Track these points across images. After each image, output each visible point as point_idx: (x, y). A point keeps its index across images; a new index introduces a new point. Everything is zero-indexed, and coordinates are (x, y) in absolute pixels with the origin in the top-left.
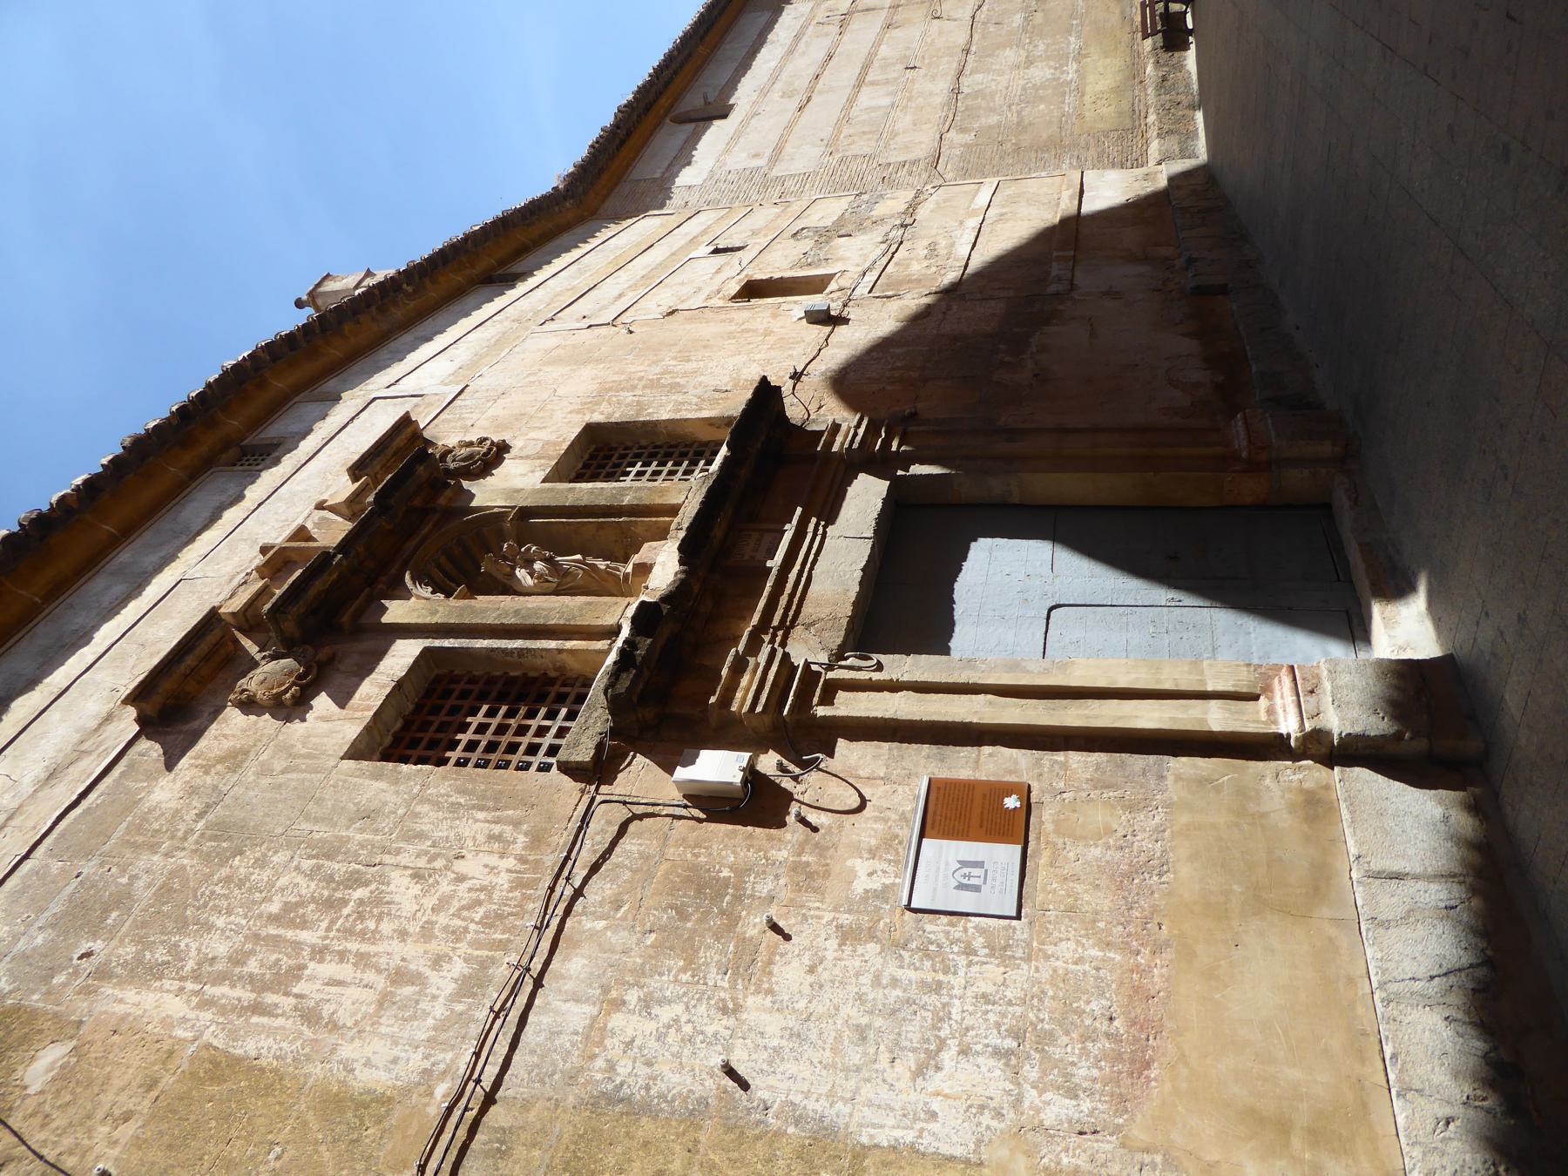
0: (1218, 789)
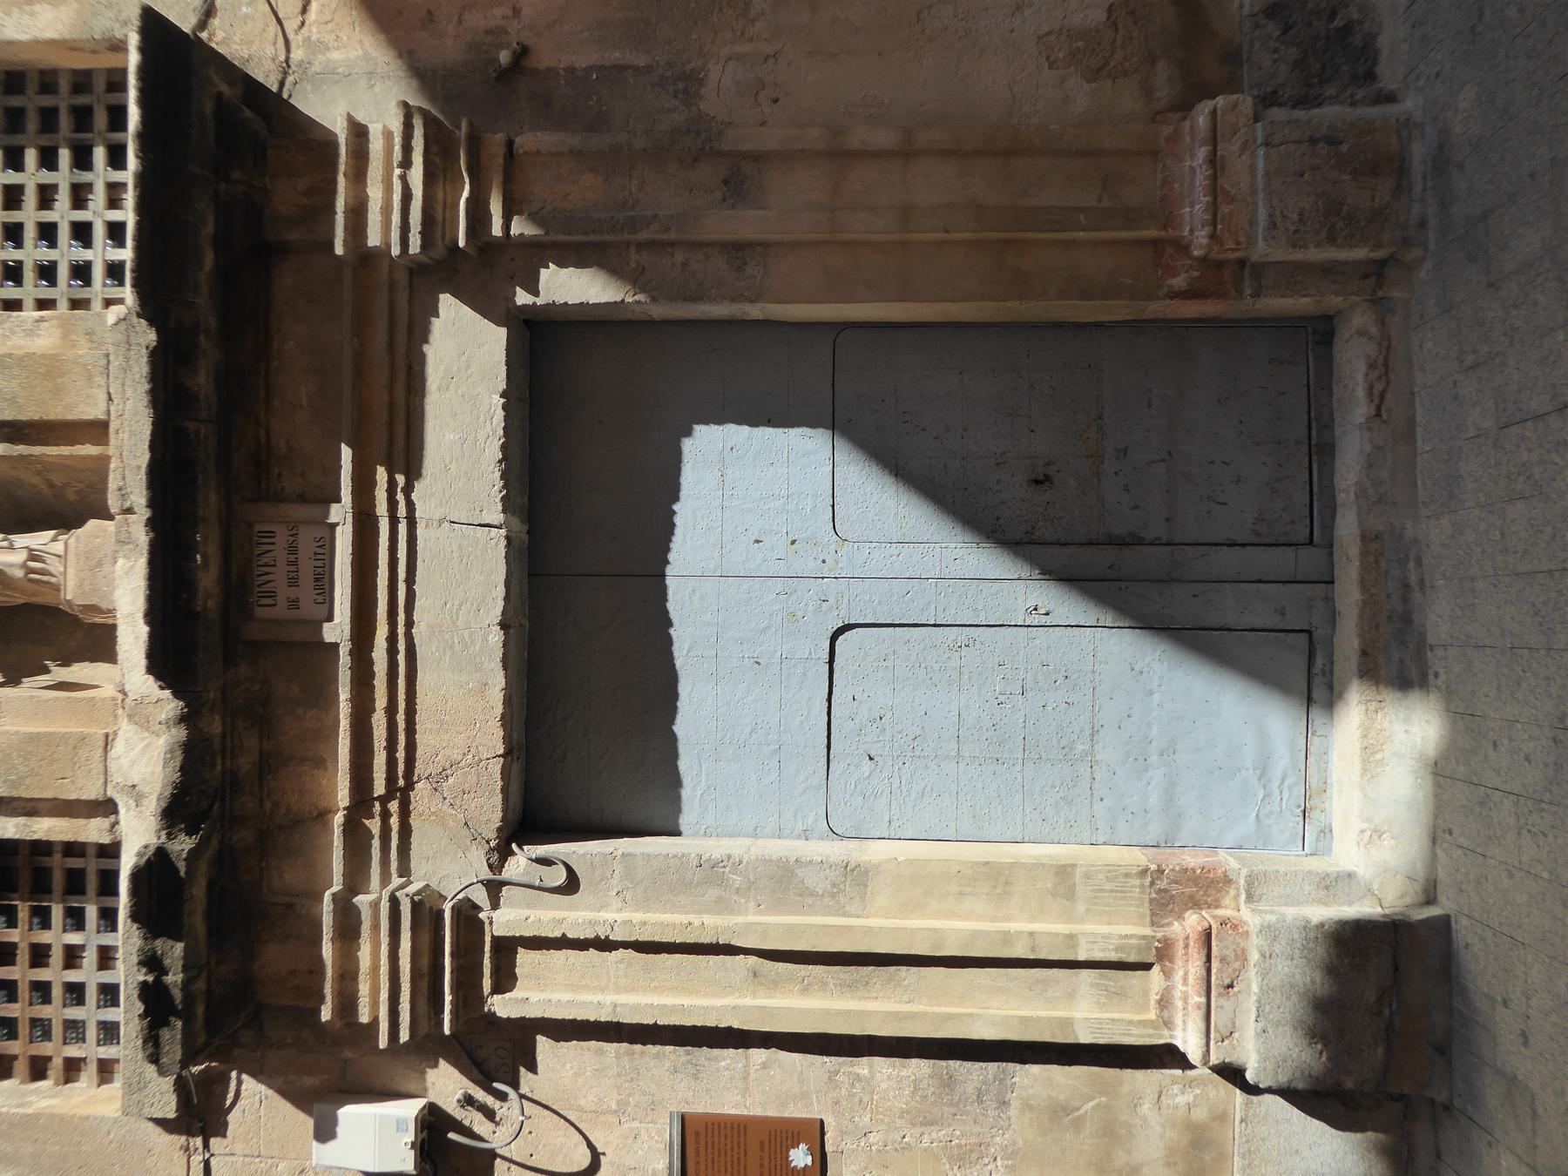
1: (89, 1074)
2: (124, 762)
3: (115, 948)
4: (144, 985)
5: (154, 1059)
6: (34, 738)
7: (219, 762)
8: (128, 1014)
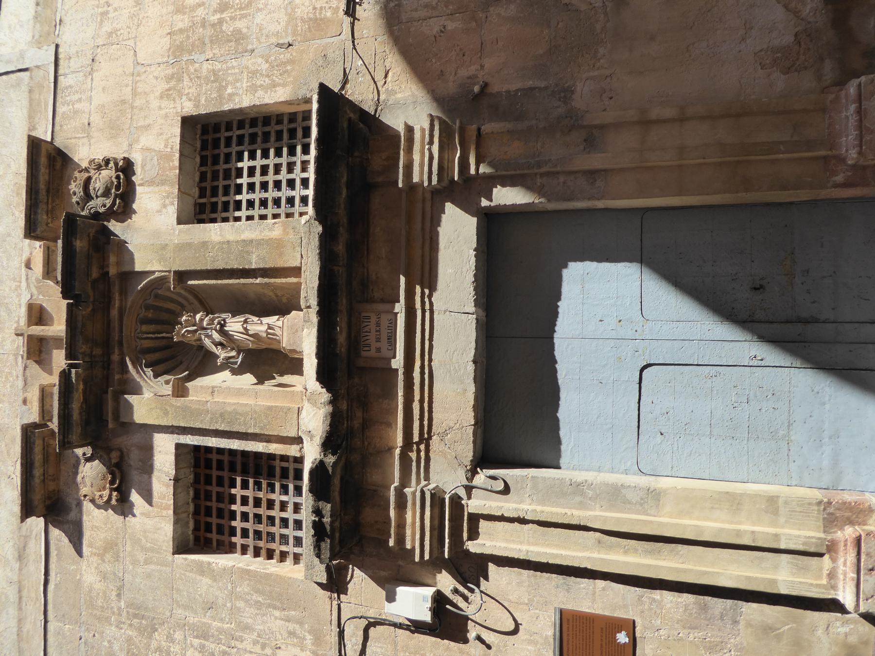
0: (779, 637)
1: (290, 560)
3: (302, 504)
4: (314, 521)
5: (318, 556)
6: (270, 408)
8: (307, 534)
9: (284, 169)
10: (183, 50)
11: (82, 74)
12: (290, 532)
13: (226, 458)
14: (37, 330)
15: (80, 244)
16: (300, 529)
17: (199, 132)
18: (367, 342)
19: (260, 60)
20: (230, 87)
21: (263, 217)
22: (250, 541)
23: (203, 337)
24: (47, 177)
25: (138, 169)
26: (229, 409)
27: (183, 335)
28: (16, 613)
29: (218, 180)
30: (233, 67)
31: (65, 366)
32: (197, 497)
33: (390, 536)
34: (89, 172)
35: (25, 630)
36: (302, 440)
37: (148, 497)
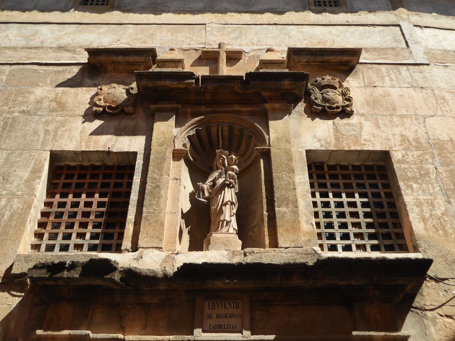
1: (35, 241)
2: (151, 254)
3: (81, 250)
4: (65, 263)
5: (35, 267)
6: (162, 224)
7: (148, 289)
8: (56, 256)
9: (357, 230)
10: (441, 150)
11: (411, 80)
12: (60, 241)
13: (123, 189)
14: (223, 57)
15: (286, 83)
16: (61, 250)
17: (379, 164)
18: (216, 306)
19: (443, 209)
20: (417, 186)
21: (316, 215)
22: (55, 209)
23: (220, 171)
24: (333, 61)
25: (345, 121)
26: (162, 192)
27: (222, 157)
28: (20, 46)
29: (343, 179)
30: (434, 188)
31: (197, 75)
32: (94, 167)
33: (45, 330)
34: (340, 88)
35: (7, 51)
36: (135, 251)
37: (97, 132)
